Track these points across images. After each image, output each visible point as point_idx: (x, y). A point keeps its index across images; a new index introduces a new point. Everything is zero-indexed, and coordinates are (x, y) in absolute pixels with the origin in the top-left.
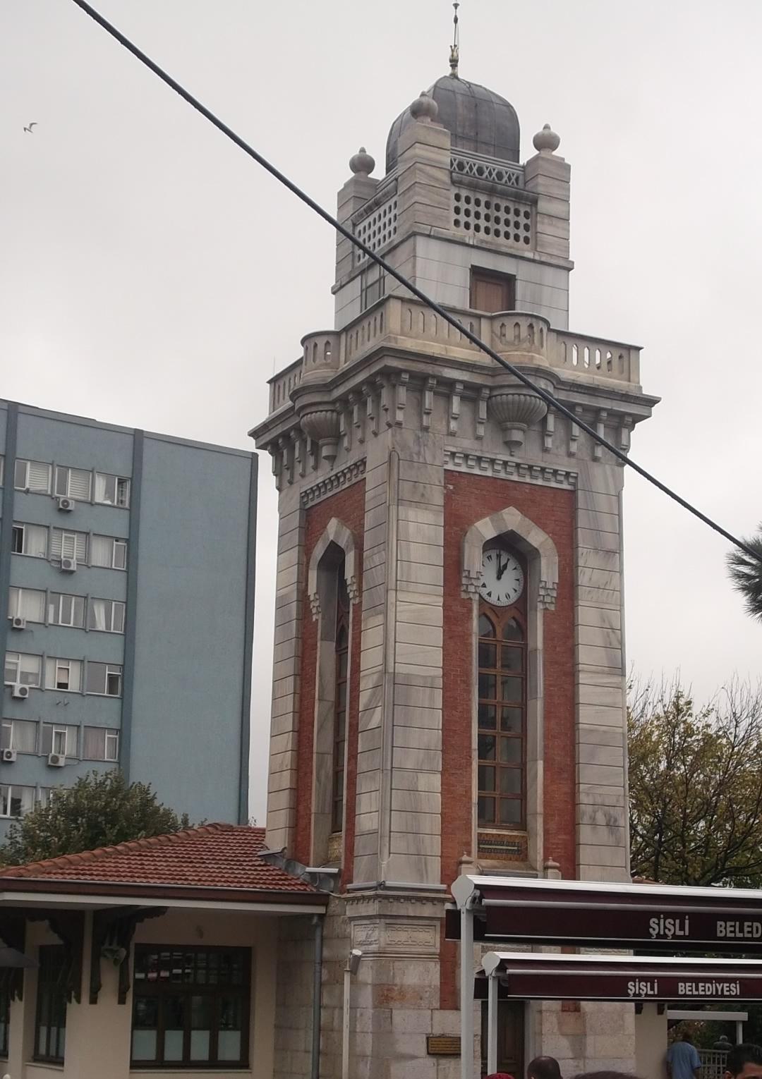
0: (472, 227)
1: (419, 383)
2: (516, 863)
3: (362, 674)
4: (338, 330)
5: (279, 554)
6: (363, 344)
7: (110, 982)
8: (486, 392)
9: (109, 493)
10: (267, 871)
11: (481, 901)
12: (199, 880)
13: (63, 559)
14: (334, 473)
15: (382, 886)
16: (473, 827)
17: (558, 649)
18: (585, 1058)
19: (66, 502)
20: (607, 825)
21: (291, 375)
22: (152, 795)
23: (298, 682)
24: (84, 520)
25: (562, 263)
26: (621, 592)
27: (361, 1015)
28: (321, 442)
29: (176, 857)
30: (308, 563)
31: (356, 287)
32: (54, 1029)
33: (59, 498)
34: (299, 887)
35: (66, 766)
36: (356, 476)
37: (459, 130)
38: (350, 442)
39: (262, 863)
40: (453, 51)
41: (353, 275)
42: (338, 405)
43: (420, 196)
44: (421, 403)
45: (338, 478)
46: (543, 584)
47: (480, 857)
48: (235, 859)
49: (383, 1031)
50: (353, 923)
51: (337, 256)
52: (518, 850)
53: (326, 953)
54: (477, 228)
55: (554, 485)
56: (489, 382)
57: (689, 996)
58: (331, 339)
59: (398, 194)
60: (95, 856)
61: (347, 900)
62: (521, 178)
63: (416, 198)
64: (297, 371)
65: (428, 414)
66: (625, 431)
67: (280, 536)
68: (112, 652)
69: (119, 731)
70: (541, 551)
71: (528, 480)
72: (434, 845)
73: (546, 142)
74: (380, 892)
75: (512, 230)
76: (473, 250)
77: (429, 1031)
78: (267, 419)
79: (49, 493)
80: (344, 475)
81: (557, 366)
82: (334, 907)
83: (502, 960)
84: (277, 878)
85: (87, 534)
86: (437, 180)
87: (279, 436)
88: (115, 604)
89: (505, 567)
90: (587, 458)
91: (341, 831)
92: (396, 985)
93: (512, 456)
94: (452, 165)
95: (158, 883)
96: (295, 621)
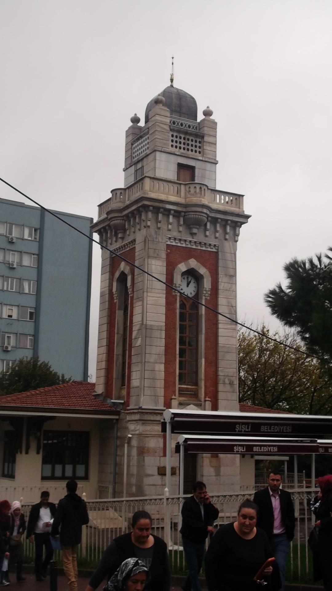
0: (178, 147)
1: (157, 211)
2: (194, 399)
3: (134, 324)
4: (125, 188)
5: (102, 274)
6: (135, 194)
7: (33, 445)
8: (183, 214)
9: (30, 235)
10: (96, 401)
11: (174, 419)
12: (69, 405)
13: (11, 263)
14: (123, 244)
15: (141, 408)
16: (177, 385)
17: (211, 314)
18: (220, 475)
19: (12, 239)
20: (230, 384)
21: (107, 204)
22: (49, 366)
23: (109, 326)
24: (19, 246)
25: (213, 161)
26: (236, 291)
27: (132, 459)
28: (118, 232)
29: (60, 396)
30: (113, 279)
31: (132, 169)
32: (11, 465)
33: (9, 237)
34: (108, 408)
35: (11, 350)
36: (132, 246)
37: (174, 108)
38: (130, 232)
39: (94, 398)
40: (171, 76)
41: (131, 165)
42: (125, 217)
43: (158, 136)
44: (157, 218)
45: (125, 246)
46: (205, 289)
47: (179, 397)
48: (83, 396)
49: (141, 465)
50: (129, 422)
51: (125, 156)
52: (194, 394)
53: (119, 434)
54: (180, 148)
55: (209, 249)
56: (184, 210)
57: (257, 452)
58: (122, 191)
59: (149, 134)
60: (28, 395)
61: (127, 413)
62: (198, 128)
63: (156, 136)
64: (109, 202)
65: (160, 222)
66: (237, 228)
67: (102, 268)
68: (31, 302)
69: (33, 336)
70: (204, 276)
71: (199, 248)
72: (161, 392)
73: (207, 113)
74: (140, 411)
75: (194, 148)
76: (179, 157)
77: (159, 465)
78: (97, 221)
79: (5, 234)
80: (127, 245)
81: (211, 203)
82: (122, 416)
83: (186, 439)
84: (100, 404)
85: (21, 252)
86: (164, 129)
87: (101, 228)
88: (33, 282)
89: (190, 282)
90: (223, 239)
91: (125, 386)
92: (146, 447)
93: (193, 238)
94: (170, 122)
95: (53, 407)
96: (107, 302)
